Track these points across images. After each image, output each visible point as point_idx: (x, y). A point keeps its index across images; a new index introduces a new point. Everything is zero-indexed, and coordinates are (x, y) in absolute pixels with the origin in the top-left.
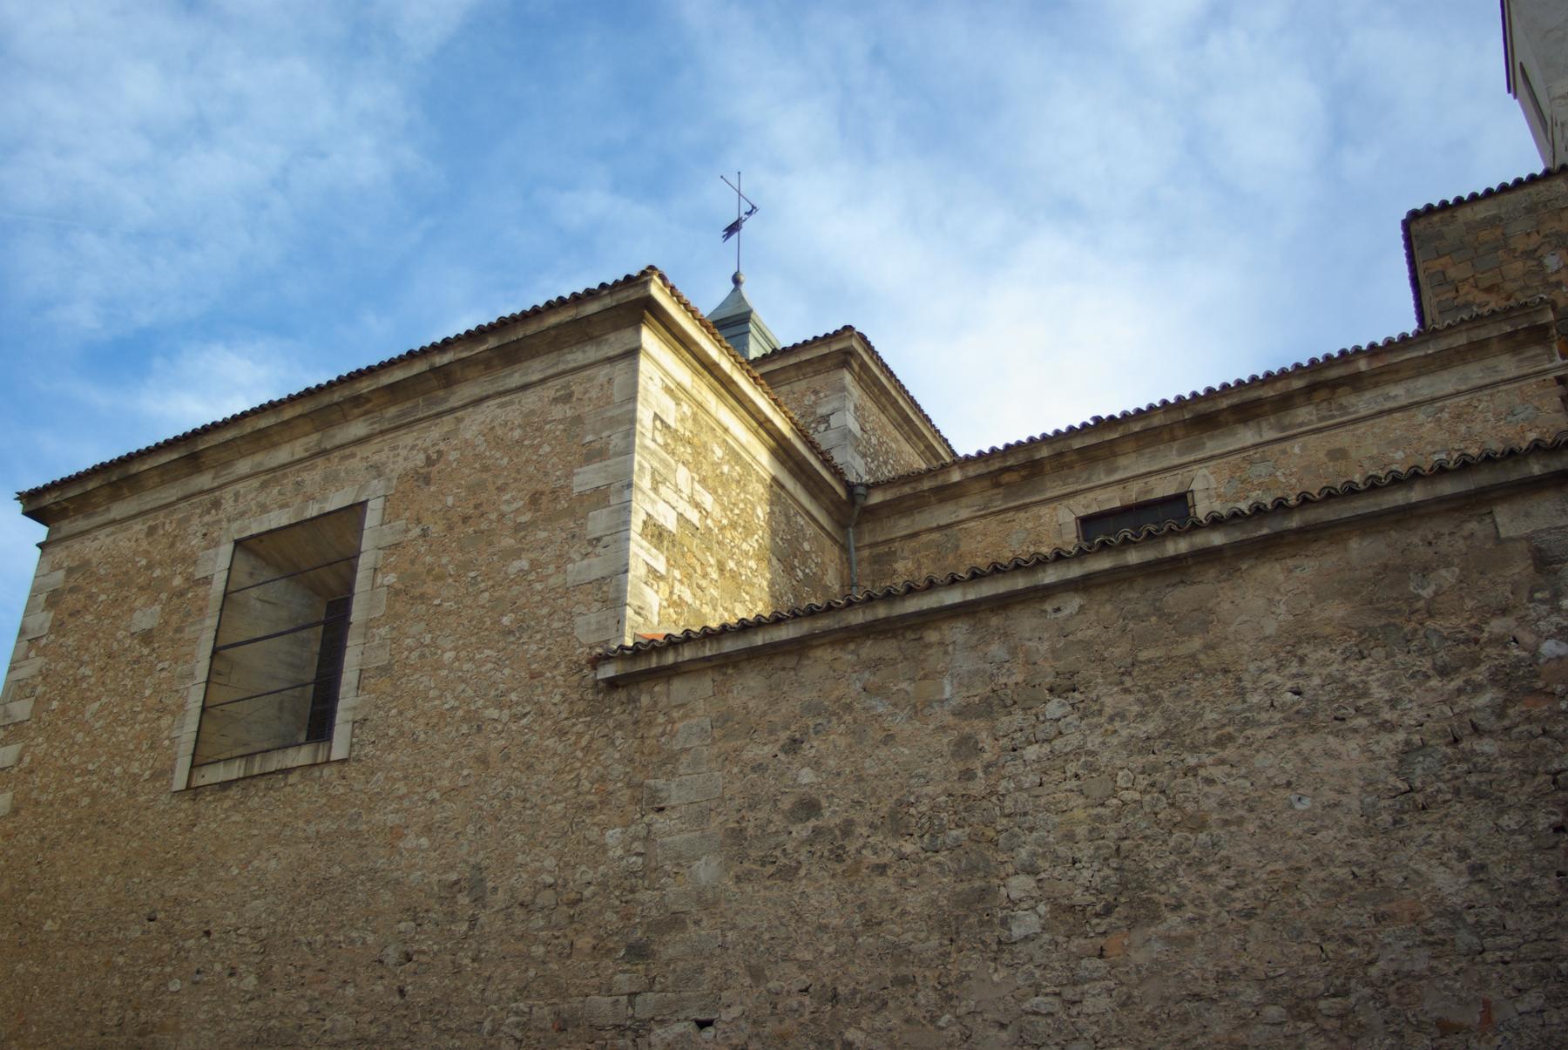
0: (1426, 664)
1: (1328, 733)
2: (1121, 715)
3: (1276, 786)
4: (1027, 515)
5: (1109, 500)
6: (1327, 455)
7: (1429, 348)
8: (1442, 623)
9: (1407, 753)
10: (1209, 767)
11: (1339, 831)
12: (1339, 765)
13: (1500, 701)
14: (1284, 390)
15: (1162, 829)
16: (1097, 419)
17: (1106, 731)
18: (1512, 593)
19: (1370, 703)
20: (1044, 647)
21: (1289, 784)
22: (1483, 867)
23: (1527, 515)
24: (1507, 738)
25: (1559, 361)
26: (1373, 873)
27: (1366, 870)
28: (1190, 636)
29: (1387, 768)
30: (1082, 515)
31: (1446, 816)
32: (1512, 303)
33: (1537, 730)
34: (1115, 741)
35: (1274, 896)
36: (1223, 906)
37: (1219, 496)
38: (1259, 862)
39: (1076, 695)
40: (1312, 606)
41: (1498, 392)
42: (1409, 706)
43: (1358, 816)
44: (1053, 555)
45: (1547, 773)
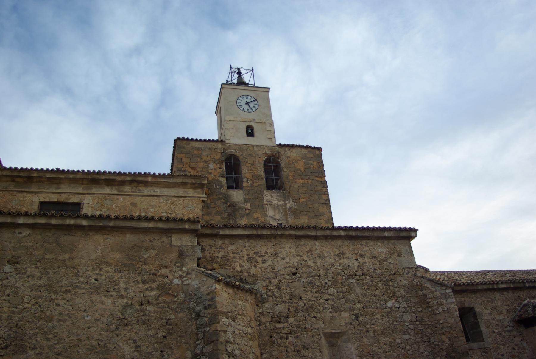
0: (139, 279)
1: (103, 295)
2: (32, 276)
3: (81, 310)
4: (22, 195)
5: (54, 198)
6: (130, 204)
7: (171, 180)
8: (148, 267)
9: (126, 306)
10: (59, 300)
11: (98, 329)
12: (103, 307)
13: (158, 295)
14: (124, 179)
15: (36, 319)
16: (58, 169)
17: (25, 280)
18: (170, 262)
19: (119, 288)
20: (11, 245)
21: (85, 310)
22: (139, 346)
23: (181, 239)
24: (157, 307)
25: (205, 195)
26: (105, 344)
27: (103, 343)
28: (66, 253)
29: (118, 310)
30: (42, 200)
31: (133, 328)
32: (197, 174)
33: (166, 305)
34: (27, 285)
35: (70, 348)
36: (50, 350)
37: (92, 207)
38: (68, 336)
39: (18, 265)
40: (109, 252)
41: (186, 199)
42: (131, 291)
43: (105, 324)
44: (25, 213)
45: (166, 319)
